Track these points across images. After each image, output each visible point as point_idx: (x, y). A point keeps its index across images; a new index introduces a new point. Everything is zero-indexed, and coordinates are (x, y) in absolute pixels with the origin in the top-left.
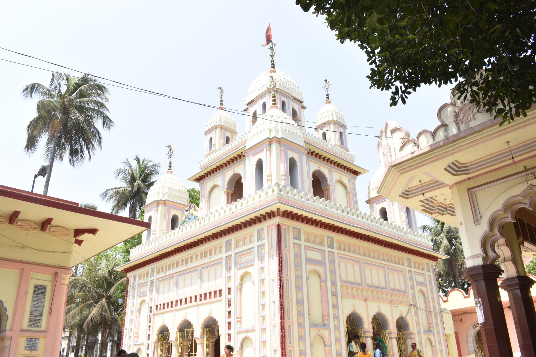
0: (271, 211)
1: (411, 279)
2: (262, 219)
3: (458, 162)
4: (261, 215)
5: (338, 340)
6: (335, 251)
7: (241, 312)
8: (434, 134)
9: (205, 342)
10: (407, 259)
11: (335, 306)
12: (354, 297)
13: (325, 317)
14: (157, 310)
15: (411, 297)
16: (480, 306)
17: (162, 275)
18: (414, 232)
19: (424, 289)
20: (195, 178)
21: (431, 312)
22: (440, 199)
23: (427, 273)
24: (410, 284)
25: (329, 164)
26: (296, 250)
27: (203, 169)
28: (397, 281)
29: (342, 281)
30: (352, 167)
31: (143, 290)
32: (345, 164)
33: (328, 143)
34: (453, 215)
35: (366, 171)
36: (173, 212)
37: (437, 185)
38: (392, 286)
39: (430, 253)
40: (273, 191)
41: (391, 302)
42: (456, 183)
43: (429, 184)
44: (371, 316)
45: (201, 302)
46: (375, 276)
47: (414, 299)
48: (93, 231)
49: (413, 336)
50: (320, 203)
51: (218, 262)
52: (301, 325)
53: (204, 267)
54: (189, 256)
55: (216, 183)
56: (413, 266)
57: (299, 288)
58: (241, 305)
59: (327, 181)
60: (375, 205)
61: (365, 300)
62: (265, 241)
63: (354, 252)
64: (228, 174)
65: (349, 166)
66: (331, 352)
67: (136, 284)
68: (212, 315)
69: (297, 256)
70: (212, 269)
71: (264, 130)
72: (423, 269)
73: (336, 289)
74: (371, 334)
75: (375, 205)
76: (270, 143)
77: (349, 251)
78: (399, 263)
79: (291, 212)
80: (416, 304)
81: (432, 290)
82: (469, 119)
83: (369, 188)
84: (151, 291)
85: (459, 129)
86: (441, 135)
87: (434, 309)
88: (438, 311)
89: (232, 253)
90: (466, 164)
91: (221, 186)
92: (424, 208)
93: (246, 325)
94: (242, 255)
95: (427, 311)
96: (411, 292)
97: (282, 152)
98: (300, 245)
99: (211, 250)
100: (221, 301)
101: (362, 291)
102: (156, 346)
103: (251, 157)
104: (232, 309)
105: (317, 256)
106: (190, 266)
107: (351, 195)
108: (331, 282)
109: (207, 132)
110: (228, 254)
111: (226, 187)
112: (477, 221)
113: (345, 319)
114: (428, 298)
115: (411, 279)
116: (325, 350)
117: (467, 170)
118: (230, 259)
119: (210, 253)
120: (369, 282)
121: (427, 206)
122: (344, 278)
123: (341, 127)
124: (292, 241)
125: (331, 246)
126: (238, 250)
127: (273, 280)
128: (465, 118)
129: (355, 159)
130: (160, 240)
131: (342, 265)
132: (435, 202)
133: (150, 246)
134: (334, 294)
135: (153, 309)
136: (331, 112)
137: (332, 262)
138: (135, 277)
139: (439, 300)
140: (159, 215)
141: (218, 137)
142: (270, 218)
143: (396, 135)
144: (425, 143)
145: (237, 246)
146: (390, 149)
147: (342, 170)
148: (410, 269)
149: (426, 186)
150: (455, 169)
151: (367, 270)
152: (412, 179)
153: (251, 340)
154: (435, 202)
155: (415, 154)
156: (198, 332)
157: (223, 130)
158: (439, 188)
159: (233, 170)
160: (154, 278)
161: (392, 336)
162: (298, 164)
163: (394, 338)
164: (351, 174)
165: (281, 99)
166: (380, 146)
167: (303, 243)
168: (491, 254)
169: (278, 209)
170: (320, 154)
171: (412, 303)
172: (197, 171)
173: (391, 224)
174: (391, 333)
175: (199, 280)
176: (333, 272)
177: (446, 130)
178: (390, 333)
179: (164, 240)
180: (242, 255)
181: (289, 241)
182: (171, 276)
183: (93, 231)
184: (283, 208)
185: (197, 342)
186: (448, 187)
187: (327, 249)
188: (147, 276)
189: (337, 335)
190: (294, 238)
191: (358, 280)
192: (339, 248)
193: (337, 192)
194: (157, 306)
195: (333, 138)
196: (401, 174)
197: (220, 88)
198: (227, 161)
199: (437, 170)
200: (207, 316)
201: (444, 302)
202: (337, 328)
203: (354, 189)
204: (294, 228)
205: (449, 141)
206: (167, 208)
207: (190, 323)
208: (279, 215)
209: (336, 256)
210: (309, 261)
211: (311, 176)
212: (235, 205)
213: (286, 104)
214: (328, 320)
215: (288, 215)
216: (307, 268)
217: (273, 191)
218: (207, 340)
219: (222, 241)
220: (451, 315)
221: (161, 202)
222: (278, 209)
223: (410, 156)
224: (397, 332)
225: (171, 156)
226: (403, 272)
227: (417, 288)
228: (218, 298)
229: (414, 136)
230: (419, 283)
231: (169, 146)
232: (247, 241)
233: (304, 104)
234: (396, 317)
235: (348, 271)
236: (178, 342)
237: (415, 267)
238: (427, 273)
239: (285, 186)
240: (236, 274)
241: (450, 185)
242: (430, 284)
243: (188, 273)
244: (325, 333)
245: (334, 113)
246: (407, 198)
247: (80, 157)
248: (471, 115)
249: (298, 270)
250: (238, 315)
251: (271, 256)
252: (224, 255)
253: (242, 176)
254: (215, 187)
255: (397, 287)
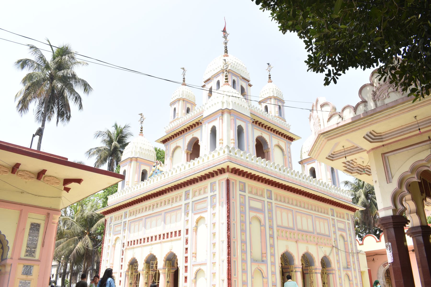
0: (222, 168)
1: (334, 225)
2: (215, 174)
3: (374, 132)
4: (214, 171)
5: (273, 273)
6: (273, 201)
7: (196, 249)
8: (355, 109)
9: (167, 272)
10: (331, 209)
11: (272, 246)
12: (287, 239)
13: (264, 254)
14: (128, 245)
15: (333, 240)
16: (390, 249)
17: (133, 217)
18: (337, 188)
19: (344, 234)
20: (161, 140)
21: (349, 253)
22: (359, 162)
23: (346, 222)
24: (332, 229)
25: (269, 131)
26: (242, 200)
27: (168, 133)
28: (322, 227)
29: (278, 226)
30: (288, 134)
31: (118, 229)
32: (283, 132)
33: (269, 114)
34: (369, 175)
35: (299, 138)
36: (143, 167)
37: (357, 150)
38: (318, 231)
39: (350, 205)
40: (224, 152)
41: (317, 244)
42: (373, 149)
43: (351, 149)
44: (301, 255)
45: (164, 240)
46: (305, 223)
47: (336, 242)
48: (79, 181)
49: (334, 272)
50: (262, 163)
51: (179, 208)
52: (244, 261)
53: (167, 212)
54: (155, 203)
55: (178, 145)
56: (335, 215)
57: (243, 231)
58: (196, 244)
59: (268, 145)
60: (306, 165)
61: (296, 242)
62: (217, 192)
63: (288, 203)
64: (188, 137)
65: (285, 133)
66: (267, 283)
67: (112, 224)
68: (172, 251)
69: (242, 205)
70: (173, 214)
71: (218, 103)
72: (344, 218)
73: (273, 232)
74: (300, 270)
75: (306, 165)
76: (223, 113)
77: (284, 202)
78: (324, 213)
79: (238, 169)
80: (337, 246)
81: (350, 235)
82: (385, 97)
83: (301, 151)
84: (124, 230)
85: (376, 105)
86: (361, 108)
87: (352, 250)
88: (355, 252)
89: (190, 201)
90: (381, 133)
91: (182, 147)
92: (345, 165)
93: (200, 259)
94: (198, 203)
95: (346, 252)
96: (333, 236)
97: (232, 120)
98: (245, 196)
99: (173, 199)
100: (180, 239)
101: (294, 234)
102: (127, 274)
103: (207, 124)
104: (189, 246)
105: (258, 205)
106: (156, 210)
107: (287, 157)
108: (269, 226)
109: (172, 104)
110: (187, 201)
111: (186, 148)
112: (389, 180)
113: (280, 256)
114: (347, 241)
115: (334, 225)
116: (263, 281)
117: (382, 138)
118: (188, 206)
119: (173, 200)
120: (299, 227)
121: (348, 167)
122: (280, 223)
123: (280, 103)
124: (239, 192)
125: (270, 198)
126: (194, 199)
127: (223, 224)
128: (381, 96)
129: (291, 127)
130: (132, 189)
131: (279, 213)
132: (355, 164)
133: (124, 194)
134: (272, 236)
135: (125, 244)
136: (272, 90)
137: (270, 211)
138: (111, 219)
139: (356, 243)
140: (132, 169)
141: (180, 108)
142: (221, 173)
143: (324, 109)
144: (349, 115)
145: (194, 196)
146: (319, 120)
147: (280, 136)
148: (333, 217)
149: (348, 150)
150: (372, 137)
151: (299, 218)
152: (337, 144)
153: (204, 271)
154: (355, 164)
155: (340, 125)
156: (161, 264)
157: (185, 102)
158: (358, 153)
159: (192, 135)
160: (127, 219)
161: (317, 271)
162: (245, 131)
163: (319, 273)
164: (288, 140)
165: (232, 78)
166: (312, 117)
167: (247, 194)
168: (400, 207)
169: (228, 166)
170: (262, 123)
171: (334, 245)
172: (163, 135)
173: (319, 181)
174: (316, 269)
175: (163, 223)
176: (271, 219)
177: (365, 106)
178: (316, 269)
179: (136, 189)
180: (198, 203)
181: (236, 192)
182: (140, 219)
183: (79, 181)
184: (232, 166)
185: (160, 272)
186: (366, 152)
187: (266, 200)
188: (121, 218)
189: (273, 270)
190: (240, 191)
191: (291, 225)
192: (276, 200)
193: (275, 154)
194: (128, 242)
195: (273, 110)
196: (328, 140)
197: (183, 69)
198: (187, 127)
199: (357, 138)
200: (169, 251)
201: (360, 245)
202: (273, 264)
203: (290, 152)
204: (240, 182)
205: (368, 114)
206: (138, 164)
207: (155, 256)
208: (228, 171)
209: (274, 205)
210: (252, 209)
211: (255, 141)
212: (193, 163)
213: (236, 82)
214: (266, 257)
215: (235, 171)
216: (250, 214)
217: (224, 152)
218: (168, 271)
219: (182, 191)
220: (365, 256)
221: (134, 158)
222: (228, 166)
223: (335, 126)
224: (321, 268)
225: (142, 122)
226: (327, 219)
227: (338, 233)
228: (178, 237)
229: (339, 110)
230: (340, 229)
231: (141, 114)
232: (202, 192)
233: (251, 83)
234: (321, 256)
235: (283, 218)
236: (144, 272)
237: (337, 216)
238: (347, 221)
239: (234, 149)
240: (193, 218)
241: (368, 150)
242: (349, 230)
243: (154, 216)
244: (263, 267)
245: (275, 90)
246: (332, 160)
247: (65, 118)
248: (386, 94)
249: (242, 216)
250: (194, 251)
251: (221, 204)
252: (183, 202)
253: (199, 139)
254: (177, 147)
255: (323, 232)
